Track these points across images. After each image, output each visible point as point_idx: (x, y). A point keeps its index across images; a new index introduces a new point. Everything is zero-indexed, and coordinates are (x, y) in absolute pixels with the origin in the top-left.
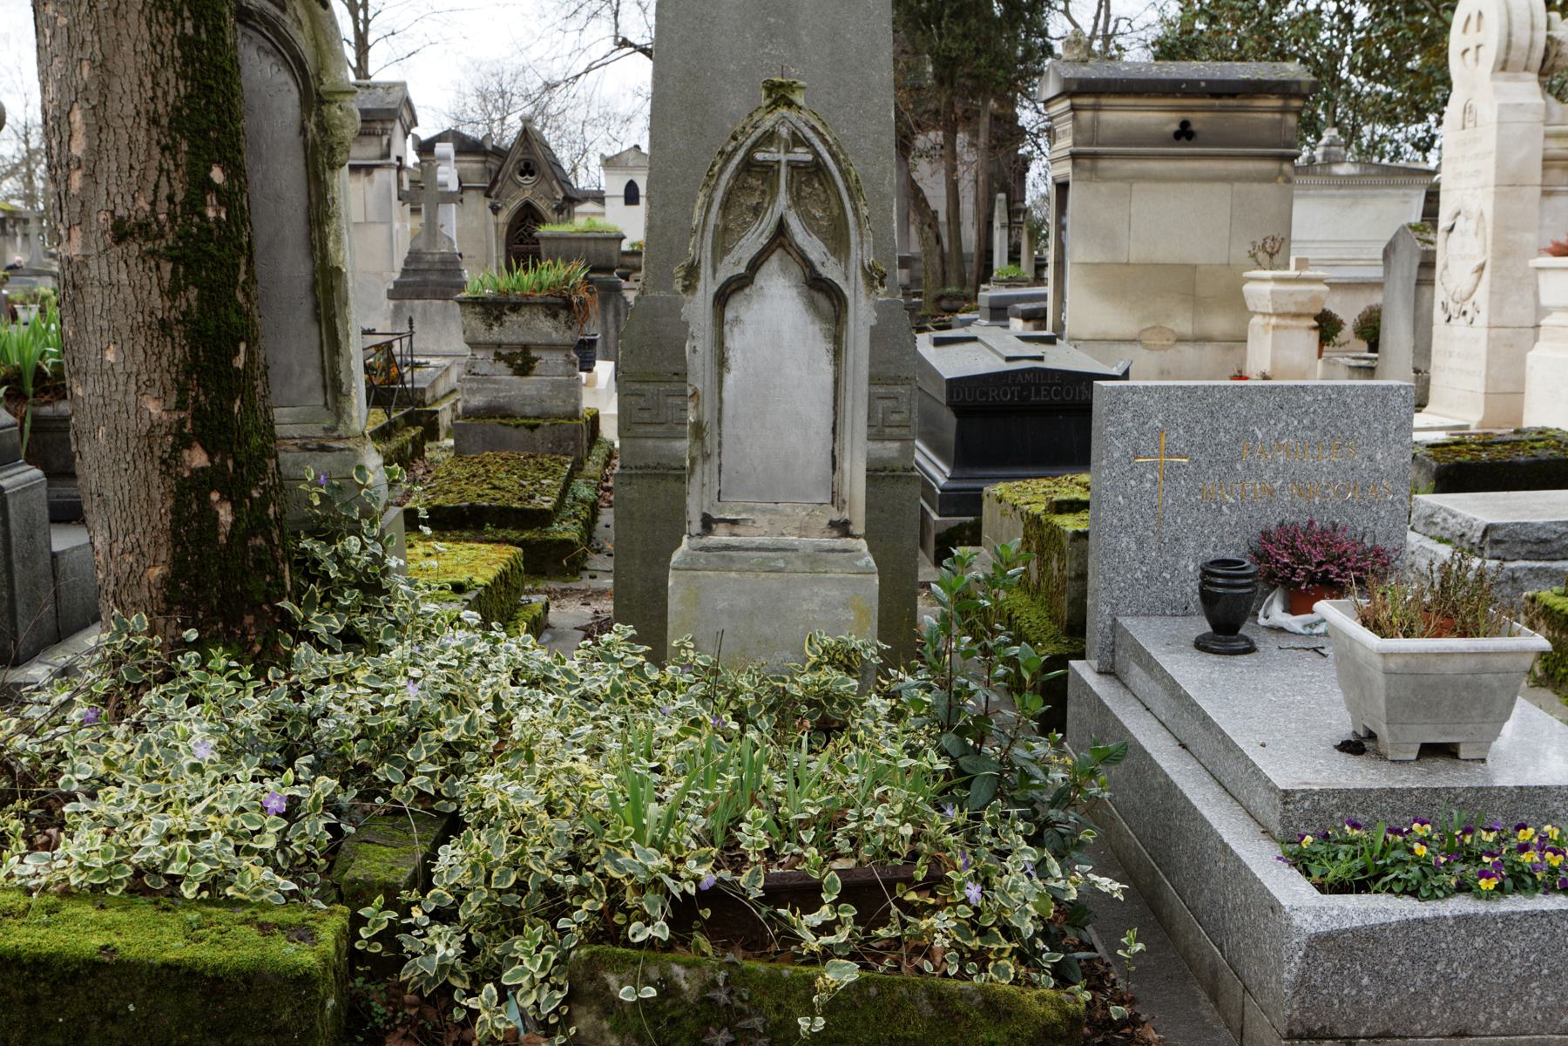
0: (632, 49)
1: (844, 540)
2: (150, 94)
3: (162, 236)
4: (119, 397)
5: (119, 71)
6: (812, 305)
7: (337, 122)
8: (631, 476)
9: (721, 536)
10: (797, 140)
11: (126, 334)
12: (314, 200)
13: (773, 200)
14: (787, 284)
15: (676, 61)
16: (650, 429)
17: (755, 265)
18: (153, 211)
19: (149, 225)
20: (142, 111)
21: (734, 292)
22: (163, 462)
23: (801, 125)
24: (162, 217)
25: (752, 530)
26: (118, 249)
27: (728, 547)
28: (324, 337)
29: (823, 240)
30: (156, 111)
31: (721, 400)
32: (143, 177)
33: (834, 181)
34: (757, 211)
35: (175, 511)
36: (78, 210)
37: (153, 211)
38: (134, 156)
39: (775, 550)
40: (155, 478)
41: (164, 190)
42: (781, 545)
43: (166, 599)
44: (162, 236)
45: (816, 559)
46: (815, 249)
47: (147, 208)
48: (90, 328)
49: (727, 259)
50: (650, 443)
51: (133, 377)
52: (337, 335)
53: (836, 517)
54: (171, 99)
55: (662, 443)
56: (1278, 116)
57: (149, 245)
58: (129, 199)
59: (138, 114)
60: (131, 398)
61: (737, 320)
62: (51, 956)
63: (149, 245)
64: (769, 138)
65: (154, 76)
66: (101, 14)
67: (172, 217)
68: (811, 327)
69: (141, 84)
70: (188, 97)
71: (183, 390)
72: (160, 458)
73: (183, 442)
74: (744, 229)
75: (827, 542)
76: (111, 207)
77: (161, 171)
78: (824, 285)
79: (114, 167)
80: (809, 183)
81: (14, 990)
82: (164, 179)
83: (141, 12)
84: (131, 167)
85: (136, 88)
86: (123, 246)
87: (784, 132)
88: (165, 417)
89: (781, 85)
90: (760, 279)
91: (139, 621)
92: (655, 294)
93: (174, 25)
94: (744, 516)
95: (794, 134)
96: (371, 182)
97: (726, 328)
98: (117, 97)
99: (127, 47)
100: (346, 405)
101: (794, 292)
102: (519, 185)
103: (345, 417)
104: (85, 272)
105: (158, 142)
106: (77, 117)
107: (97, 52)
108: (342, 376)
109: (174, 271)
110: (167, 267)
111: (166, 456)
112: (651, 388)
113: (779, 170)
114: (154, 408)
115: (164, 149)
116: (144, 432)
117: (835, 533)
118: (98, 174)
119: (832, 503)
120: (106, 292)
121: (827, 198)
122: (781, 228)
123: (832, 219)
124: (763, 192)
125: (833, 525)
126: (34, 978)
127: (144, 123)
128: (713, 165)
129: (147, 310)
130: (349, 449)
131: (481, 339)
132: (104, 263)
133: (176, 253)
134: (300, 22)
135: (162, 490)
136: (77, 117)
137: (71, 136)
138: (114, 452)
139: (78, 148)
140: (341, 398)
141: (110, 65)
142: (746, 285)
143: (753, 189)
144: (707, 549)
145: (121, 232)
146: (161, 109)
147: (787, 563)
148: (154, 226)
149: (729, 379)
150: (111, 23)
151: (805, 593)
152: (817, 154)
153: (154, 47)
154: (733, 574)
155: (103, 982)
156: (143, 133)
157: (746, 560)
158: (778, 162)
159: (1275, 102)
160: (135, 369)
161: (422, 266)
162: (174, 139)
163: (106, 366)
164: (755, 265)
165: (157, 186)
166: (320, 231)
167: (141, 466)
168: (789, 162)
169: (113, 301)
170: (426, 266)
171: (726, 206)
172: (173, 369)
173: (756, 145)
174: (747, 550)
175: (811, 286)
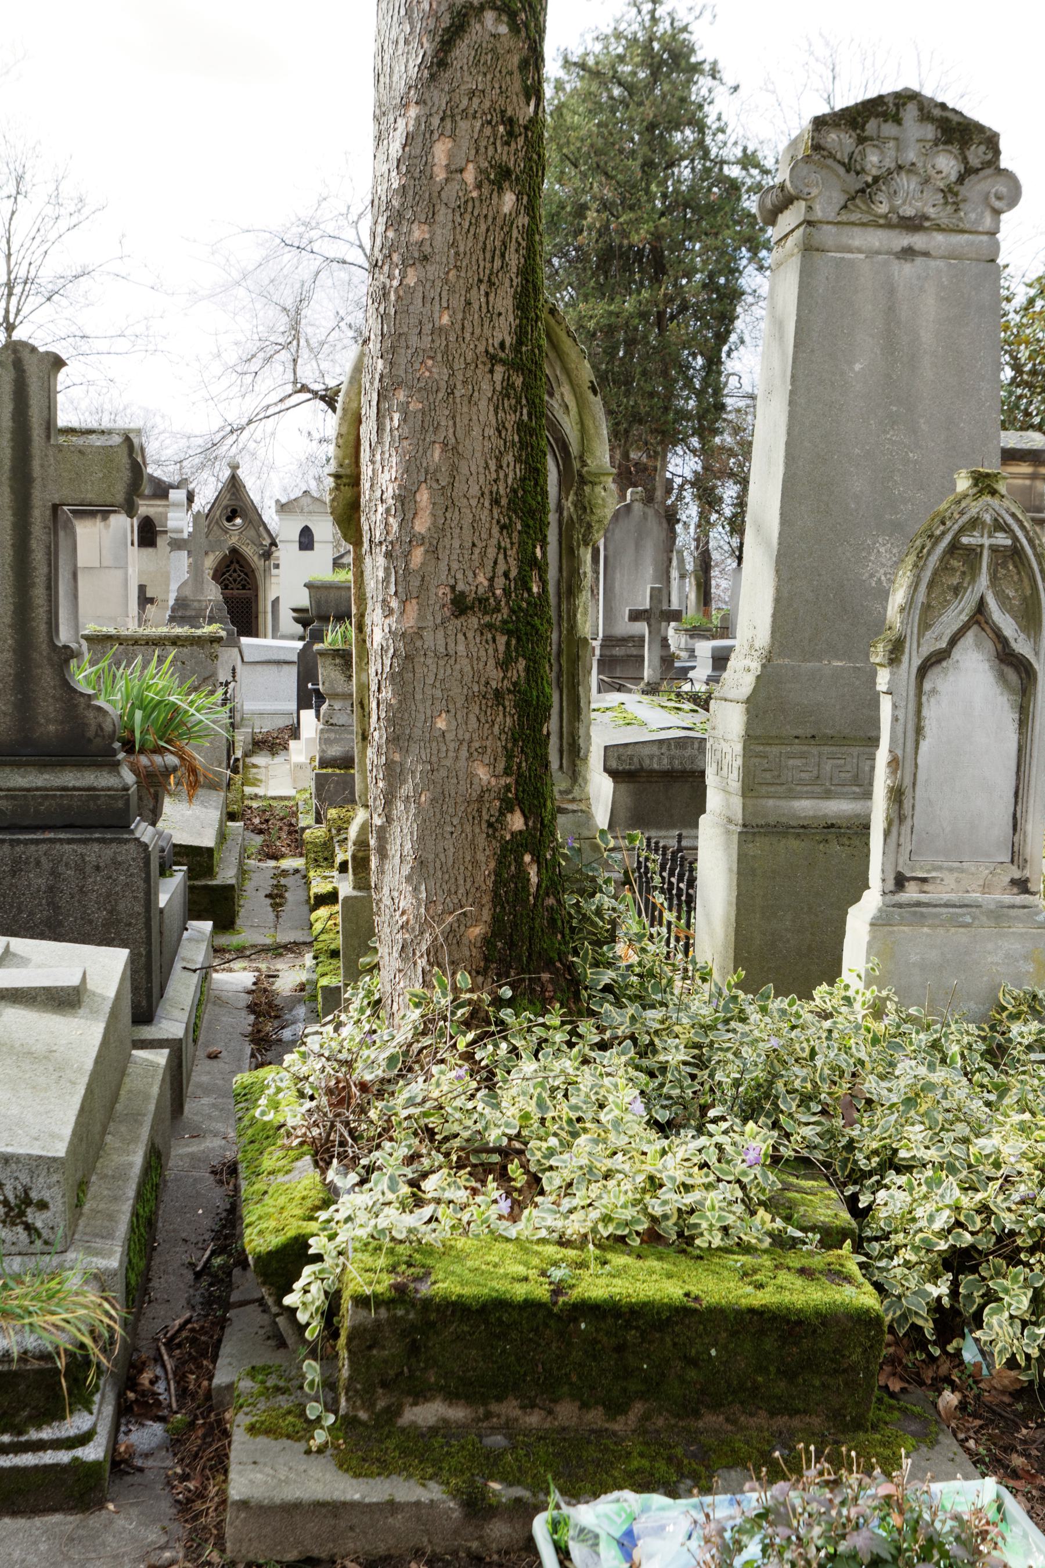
0: (309, 396)
1: (1023, 896)
2: (494, 476)
3: (497, 610)
4: (448, 763)
5: (467, 454)
6: (1002, 677)
7: (600, 502)
8: (754, 834)
9: (911, 893)
10: (999, 526)
11: (460, 701)
12: (565, 574)
13: (973, 580)
14: (981, 658)
15: (807, 444)
16: (772, 789)
17: (953, 641)
18: (491, 586)
19: (487, 599)
20: (487, 491)
21: (932, 665)
22: (490, 825)
23: (1003, 513)
24: (498, 592)
25: (940, 888)
26: (458, 622)
27: (918, 904)
28: (565, 704)
29: (1014, 618)
30: (497, 493)
31: (916, 765)
32: (483, 554)
33: (1030, 565)
34: (957, 590)
35: (497, 874)
36: (417, 584)
37: (491, 586)
38: (477, 534)
39: (961, 906)
40: (481, 840)
41: (501, 568)
42: (966, 902)
43: (487, 959)
44: (497, 610)
45: (999, 915)
46: (1008, 626)
47: (486, 583)
48: (419, 696)
49: (928, 634)
50: (771, 802)
51: (465, 744)
52: (579, 702)
53: (1017, 875)
54: (510, 482)
55: (782, 803)
56: (1028, 482)
57: (487, 618)
58: (470, 574)
59: (482, 495)
60: (462, 763)
61: (934, 691)
62: (645, 1304)
63: (487, 618)
64: (975, 523)
65: (498, 459)
66: (458, 400)
67: (506, 592)
68: (1000, 698)
69: (487, 467)
70: (523, 479)
71: (510, 757)
72: (488, 821)
73: (507, 807)
74: (944, 607)
75: (1008, 898)
76: (452, 582)
77: (499, 548)
78: (1014, 660)
79: (456, 543)
80: (1004, 565)
81: (605, 1339)
82: (501, 556)
83: (490, 399)
84: (474, 545)
85: (481, 470)
86: (462, 619)
87: (987, 518)
88: (493, 781)
89: (988, 475)
90: (957, 654)
91: (464, 979)
92: (779, 662)
93: (515, 412)
94: (934, 874)
95: (996, 520)
96: (108, 527)
97: (924, 699)
98: (464, 479)
99: (476, 432)
100: (582, 769)
101: (986, 666)
102: (226, 531)
103: (580, 780)
104: (419, 643)
105: (498, 522)
106: (424, 497)
107: (451, 436)
108: (581, 741)
109: (508, 644)
110: (502, 640)
111: (493, 819)
112: (775, 750)
113: (981, 553)
114: (483, 773)
115: (503, 527)
116: (475, 796)
117: (1015, 890)
118: (440, 551)
119: (1012, 862)
120: (442, 663)
121: (1021, 580)
122: (981, 606)
123: (1024, 599)
124: (964, 573)
125: (1014, 882)
126: (628, 1326)
127: (487, 504)
128: (923, 547)
129: (483, 680)
130: (582, 811)
131: (339, 690)
132: (440, 633)
133: (510, 626)
134: (567, 407)
135: (487, 853)
136: (424, 497)
137: (415, 514)
138: (438, 816)
139: (422, 525)
140: (578, 762)
141: (460, 448)
142: (944, 659)
143: (954, 570)
144: (899, 906)
145: (460, 605)
146: (502, 492)
147: (974, 918)
148: (492, 600)
149: (924, 746)
150: (465, 409)
151: (990, 946)
152: (1016, 539)
153: (500, 432)
154: (926, 930)
155: (689, 1328)
156: (486, 512)
157: (937, 916)
158: (982, 546)
159: (1025, 469)
160: (467, 736)
161: (189, 613)
162: (510, 518)
163: (437, 734)
164: (953, 641)
165: (495, 563)
166: (569, 602)
167: (468, 829)
168: (991, 546)
169: (449, 671)
170: (193, 613)
171: (931, 585)
172: (503, 737)
173: (962, 531)
174: (935, 906)
175: (1001, 661)
